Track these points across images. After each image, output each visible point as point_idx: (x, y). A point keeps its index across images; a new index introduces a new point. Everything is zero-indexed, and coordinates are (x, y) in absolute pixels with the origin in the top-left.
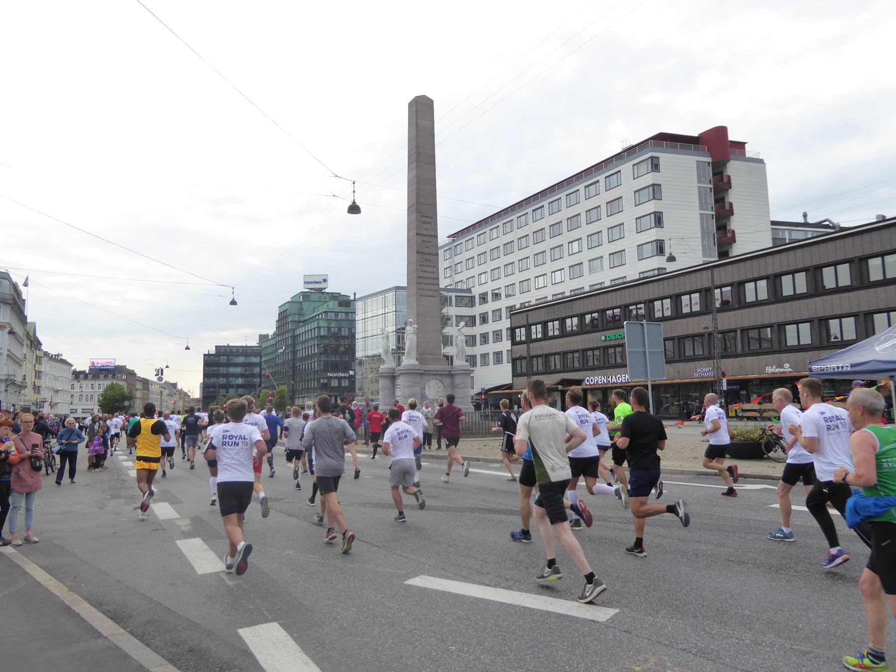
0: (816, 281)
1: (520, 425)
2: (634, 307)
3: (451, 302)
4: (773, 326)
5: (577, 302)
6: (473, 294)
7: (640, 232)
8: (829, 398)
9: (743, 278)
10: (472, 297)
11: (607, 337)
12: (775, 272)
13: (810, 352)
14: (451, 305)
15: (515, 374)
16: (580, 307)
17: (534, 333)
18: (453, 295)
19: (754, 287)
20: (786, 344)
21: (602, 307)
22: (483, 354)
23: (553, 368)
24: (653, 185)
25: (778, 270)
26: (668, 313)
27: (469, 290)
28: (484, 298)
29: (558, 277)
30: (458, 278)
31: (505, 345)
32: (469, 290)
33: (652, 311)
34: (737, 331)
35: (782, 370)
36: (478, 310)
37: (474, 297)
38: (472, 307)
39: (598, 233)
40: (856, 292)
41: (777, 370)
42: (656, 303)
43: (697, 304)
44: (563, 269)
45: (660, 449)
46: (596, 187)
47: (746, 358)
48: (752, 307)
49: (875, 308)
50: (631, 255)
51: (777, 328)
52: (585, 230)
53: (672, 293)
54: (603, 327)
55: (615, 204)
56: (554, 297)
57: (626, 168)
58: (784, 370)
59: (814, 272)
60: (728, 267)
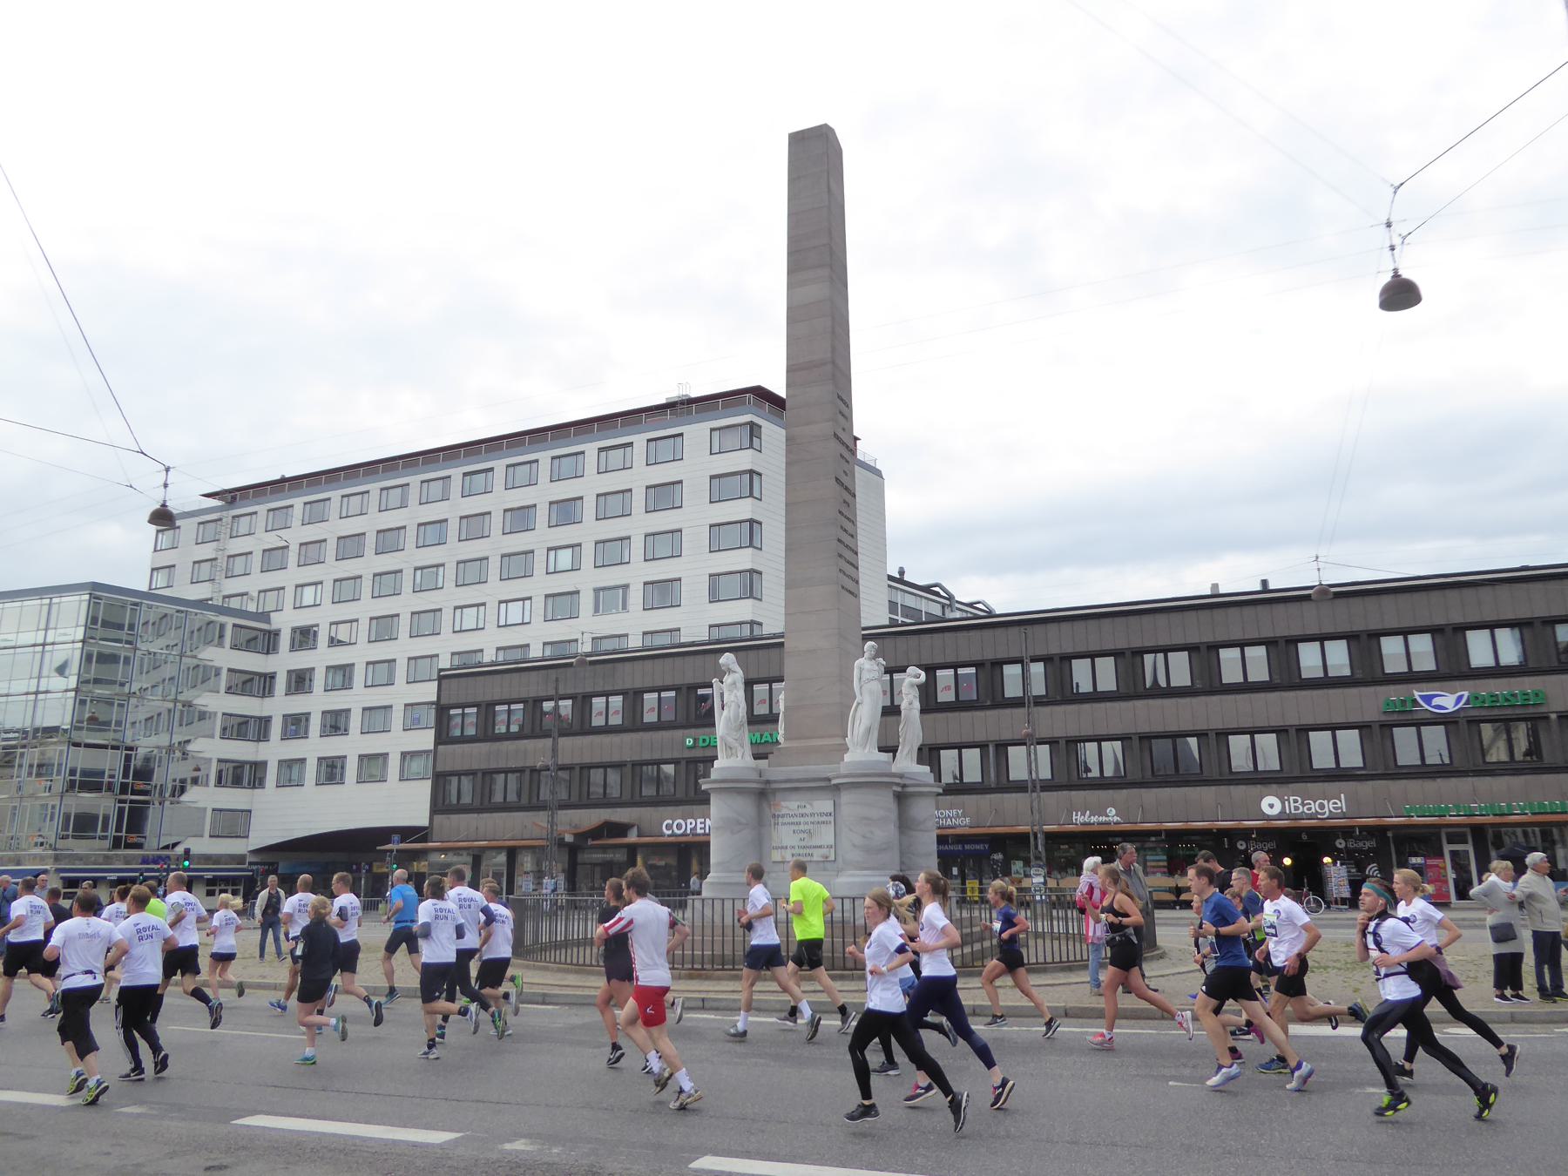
0: (634, 712)
1: (874, 934)
2: (459, 711)
3: (221, 636)
4: (1058, 742)
5: (628, 665)
6: (274, 627)
7: (600, 567)
8: (1155, 870)
9: (1001, 655)
10: (269, 632)
11: (701, 741)
12: (1063, 652)
13: (1124, 791)
14: (221, 644)
15: (439, 805)
16: (630, 677)
17: (763, 701)
18: (230, 621)
19: (1020, 672)
20: (1008, 777)
21: (488, 698)
22: (285, 761)
23: (454, 801)
24: (751, 472)
25: (1068, 649)
26: (471, 731)
27: (265, 617)
28: (305, 637)
29: (515, 612)
30: (232, 586)
31: (425, 739)
32: (265, 617)
33: (1140, 671)
34: (987, 746)
35: (1102, 819)
36: (283, 662)
37: (277, 633)
38: (268, 653)
39: (355, 578)
40: (1203, 698)
41: (1094, 819)
42: (595, 700)
43: (949, 689)
44: (530, 598)
45: (1456, 989)
46: (174, 534)
47: (1006, 795)
48: (956, 711)
49: (1311, 721)
50: (694, 589)
51: (1064, 746)
52: (332, 569)
53: (628, 686)
54: (533, 730)
55: (664, 495)
56: (501, 653)
57: (696, 433)
58: (1107, 819)
59: (1058, 664)
60: (453, 680)
